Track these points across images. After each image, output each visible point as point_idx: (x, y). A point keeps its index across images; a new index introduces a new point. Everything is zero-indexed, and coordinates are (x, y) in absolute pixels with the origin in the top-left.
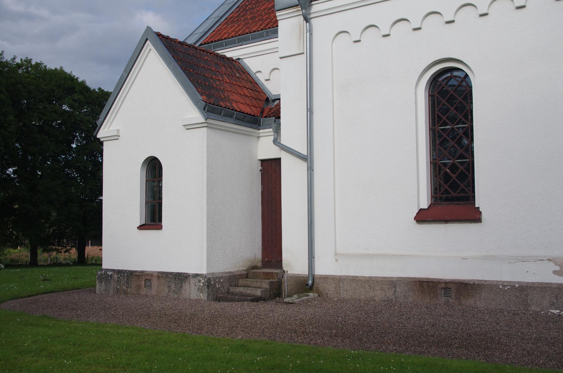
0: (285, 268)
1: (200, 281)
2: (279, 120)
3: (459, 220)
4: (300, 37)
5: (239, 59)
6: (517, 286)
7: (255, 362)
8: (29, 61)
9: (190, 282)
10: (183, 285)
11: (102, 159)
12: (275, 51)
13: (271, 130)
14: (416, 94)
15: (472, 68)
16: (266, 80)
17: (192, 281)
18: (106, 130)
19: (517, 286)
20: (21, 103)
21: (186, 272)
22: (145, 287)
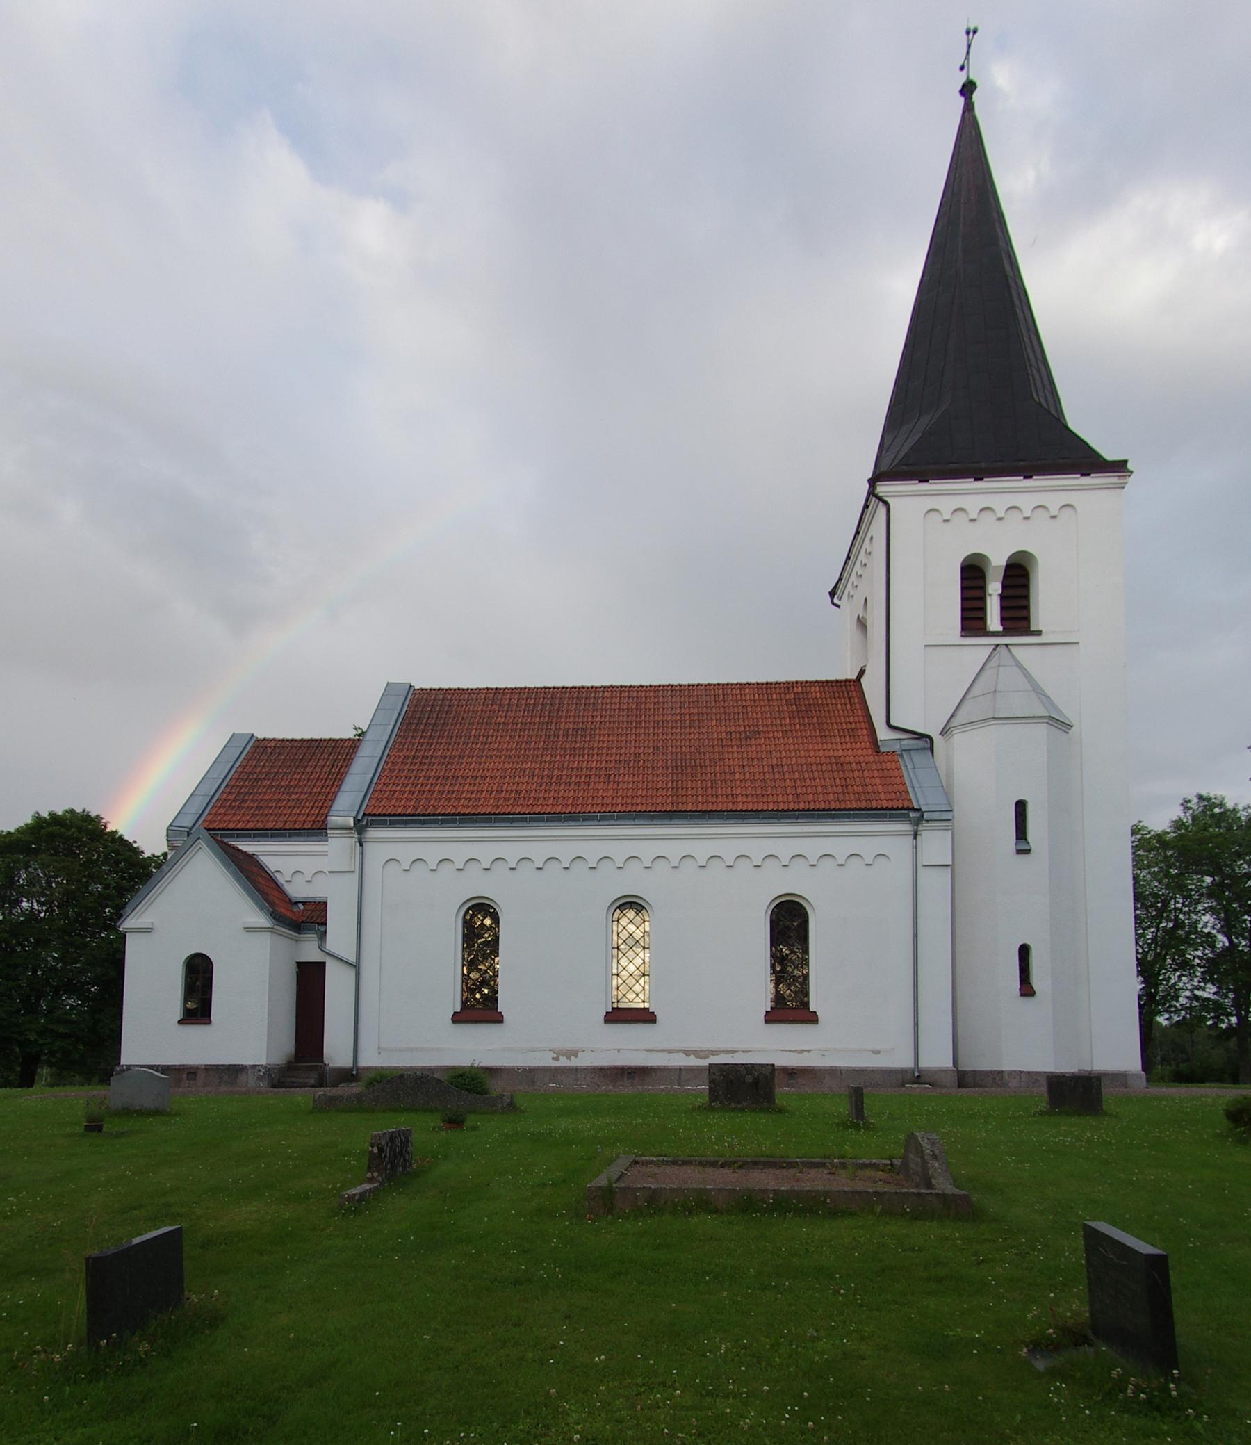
0: (326, 1060)
1: (260, 1071)
2: (1009, 563)
3: (947, 796)
4: (352, 857)
5: (254, 854)
6: (527, 1068)
7: (973, 1353)
8: (72, 811)
9: (247, 1073)
10: (239, 1075)
11: (464, 931)
12: (324, 854)
13: (315, 936)
14: (456, 921)
15: (647, 899)
16: (287, 881)
17: (250, 1071)
18: (133, 921)
19: (527, 1068)
20: (399, 1255)
21: (241, 1063)
22: (187, 1079)
